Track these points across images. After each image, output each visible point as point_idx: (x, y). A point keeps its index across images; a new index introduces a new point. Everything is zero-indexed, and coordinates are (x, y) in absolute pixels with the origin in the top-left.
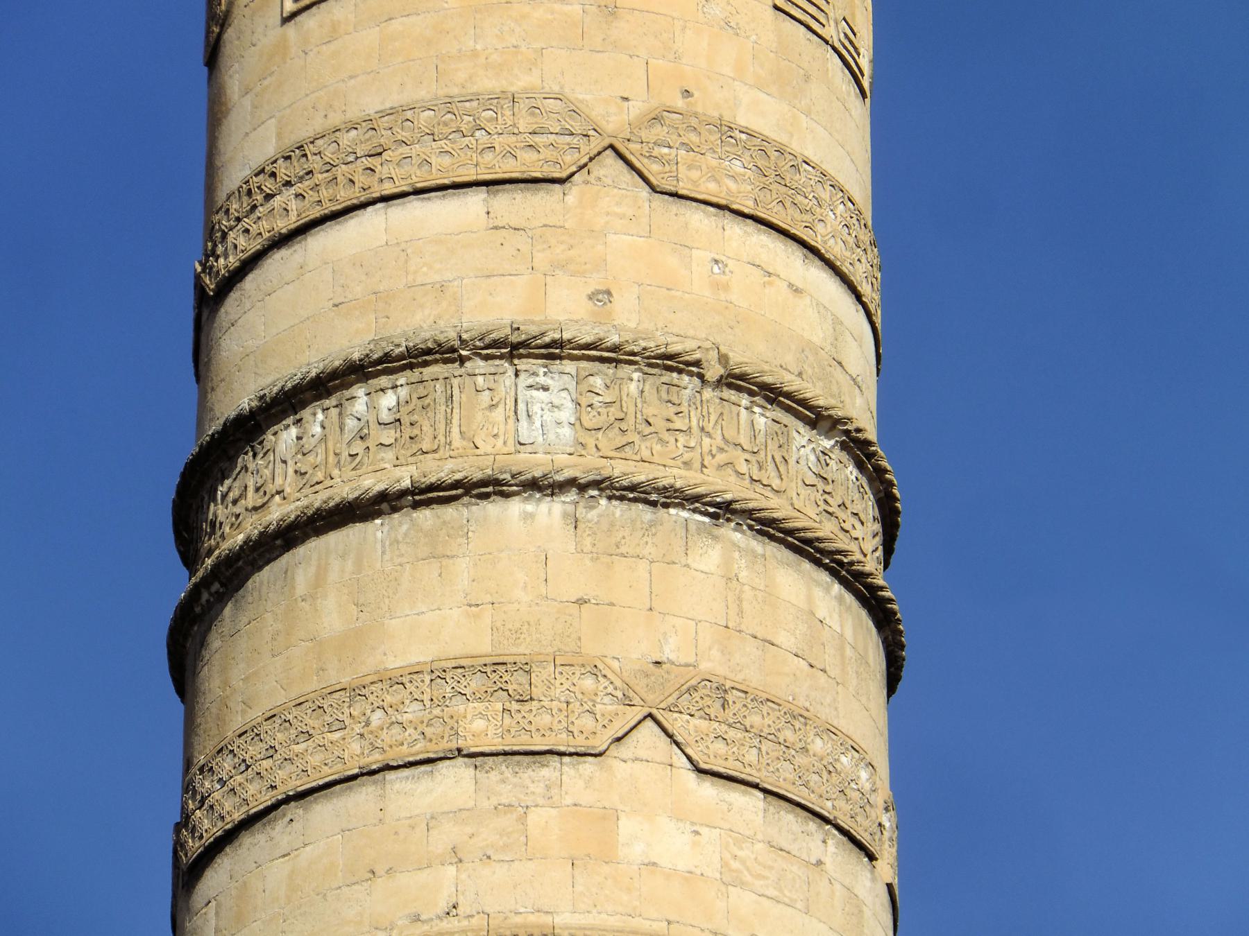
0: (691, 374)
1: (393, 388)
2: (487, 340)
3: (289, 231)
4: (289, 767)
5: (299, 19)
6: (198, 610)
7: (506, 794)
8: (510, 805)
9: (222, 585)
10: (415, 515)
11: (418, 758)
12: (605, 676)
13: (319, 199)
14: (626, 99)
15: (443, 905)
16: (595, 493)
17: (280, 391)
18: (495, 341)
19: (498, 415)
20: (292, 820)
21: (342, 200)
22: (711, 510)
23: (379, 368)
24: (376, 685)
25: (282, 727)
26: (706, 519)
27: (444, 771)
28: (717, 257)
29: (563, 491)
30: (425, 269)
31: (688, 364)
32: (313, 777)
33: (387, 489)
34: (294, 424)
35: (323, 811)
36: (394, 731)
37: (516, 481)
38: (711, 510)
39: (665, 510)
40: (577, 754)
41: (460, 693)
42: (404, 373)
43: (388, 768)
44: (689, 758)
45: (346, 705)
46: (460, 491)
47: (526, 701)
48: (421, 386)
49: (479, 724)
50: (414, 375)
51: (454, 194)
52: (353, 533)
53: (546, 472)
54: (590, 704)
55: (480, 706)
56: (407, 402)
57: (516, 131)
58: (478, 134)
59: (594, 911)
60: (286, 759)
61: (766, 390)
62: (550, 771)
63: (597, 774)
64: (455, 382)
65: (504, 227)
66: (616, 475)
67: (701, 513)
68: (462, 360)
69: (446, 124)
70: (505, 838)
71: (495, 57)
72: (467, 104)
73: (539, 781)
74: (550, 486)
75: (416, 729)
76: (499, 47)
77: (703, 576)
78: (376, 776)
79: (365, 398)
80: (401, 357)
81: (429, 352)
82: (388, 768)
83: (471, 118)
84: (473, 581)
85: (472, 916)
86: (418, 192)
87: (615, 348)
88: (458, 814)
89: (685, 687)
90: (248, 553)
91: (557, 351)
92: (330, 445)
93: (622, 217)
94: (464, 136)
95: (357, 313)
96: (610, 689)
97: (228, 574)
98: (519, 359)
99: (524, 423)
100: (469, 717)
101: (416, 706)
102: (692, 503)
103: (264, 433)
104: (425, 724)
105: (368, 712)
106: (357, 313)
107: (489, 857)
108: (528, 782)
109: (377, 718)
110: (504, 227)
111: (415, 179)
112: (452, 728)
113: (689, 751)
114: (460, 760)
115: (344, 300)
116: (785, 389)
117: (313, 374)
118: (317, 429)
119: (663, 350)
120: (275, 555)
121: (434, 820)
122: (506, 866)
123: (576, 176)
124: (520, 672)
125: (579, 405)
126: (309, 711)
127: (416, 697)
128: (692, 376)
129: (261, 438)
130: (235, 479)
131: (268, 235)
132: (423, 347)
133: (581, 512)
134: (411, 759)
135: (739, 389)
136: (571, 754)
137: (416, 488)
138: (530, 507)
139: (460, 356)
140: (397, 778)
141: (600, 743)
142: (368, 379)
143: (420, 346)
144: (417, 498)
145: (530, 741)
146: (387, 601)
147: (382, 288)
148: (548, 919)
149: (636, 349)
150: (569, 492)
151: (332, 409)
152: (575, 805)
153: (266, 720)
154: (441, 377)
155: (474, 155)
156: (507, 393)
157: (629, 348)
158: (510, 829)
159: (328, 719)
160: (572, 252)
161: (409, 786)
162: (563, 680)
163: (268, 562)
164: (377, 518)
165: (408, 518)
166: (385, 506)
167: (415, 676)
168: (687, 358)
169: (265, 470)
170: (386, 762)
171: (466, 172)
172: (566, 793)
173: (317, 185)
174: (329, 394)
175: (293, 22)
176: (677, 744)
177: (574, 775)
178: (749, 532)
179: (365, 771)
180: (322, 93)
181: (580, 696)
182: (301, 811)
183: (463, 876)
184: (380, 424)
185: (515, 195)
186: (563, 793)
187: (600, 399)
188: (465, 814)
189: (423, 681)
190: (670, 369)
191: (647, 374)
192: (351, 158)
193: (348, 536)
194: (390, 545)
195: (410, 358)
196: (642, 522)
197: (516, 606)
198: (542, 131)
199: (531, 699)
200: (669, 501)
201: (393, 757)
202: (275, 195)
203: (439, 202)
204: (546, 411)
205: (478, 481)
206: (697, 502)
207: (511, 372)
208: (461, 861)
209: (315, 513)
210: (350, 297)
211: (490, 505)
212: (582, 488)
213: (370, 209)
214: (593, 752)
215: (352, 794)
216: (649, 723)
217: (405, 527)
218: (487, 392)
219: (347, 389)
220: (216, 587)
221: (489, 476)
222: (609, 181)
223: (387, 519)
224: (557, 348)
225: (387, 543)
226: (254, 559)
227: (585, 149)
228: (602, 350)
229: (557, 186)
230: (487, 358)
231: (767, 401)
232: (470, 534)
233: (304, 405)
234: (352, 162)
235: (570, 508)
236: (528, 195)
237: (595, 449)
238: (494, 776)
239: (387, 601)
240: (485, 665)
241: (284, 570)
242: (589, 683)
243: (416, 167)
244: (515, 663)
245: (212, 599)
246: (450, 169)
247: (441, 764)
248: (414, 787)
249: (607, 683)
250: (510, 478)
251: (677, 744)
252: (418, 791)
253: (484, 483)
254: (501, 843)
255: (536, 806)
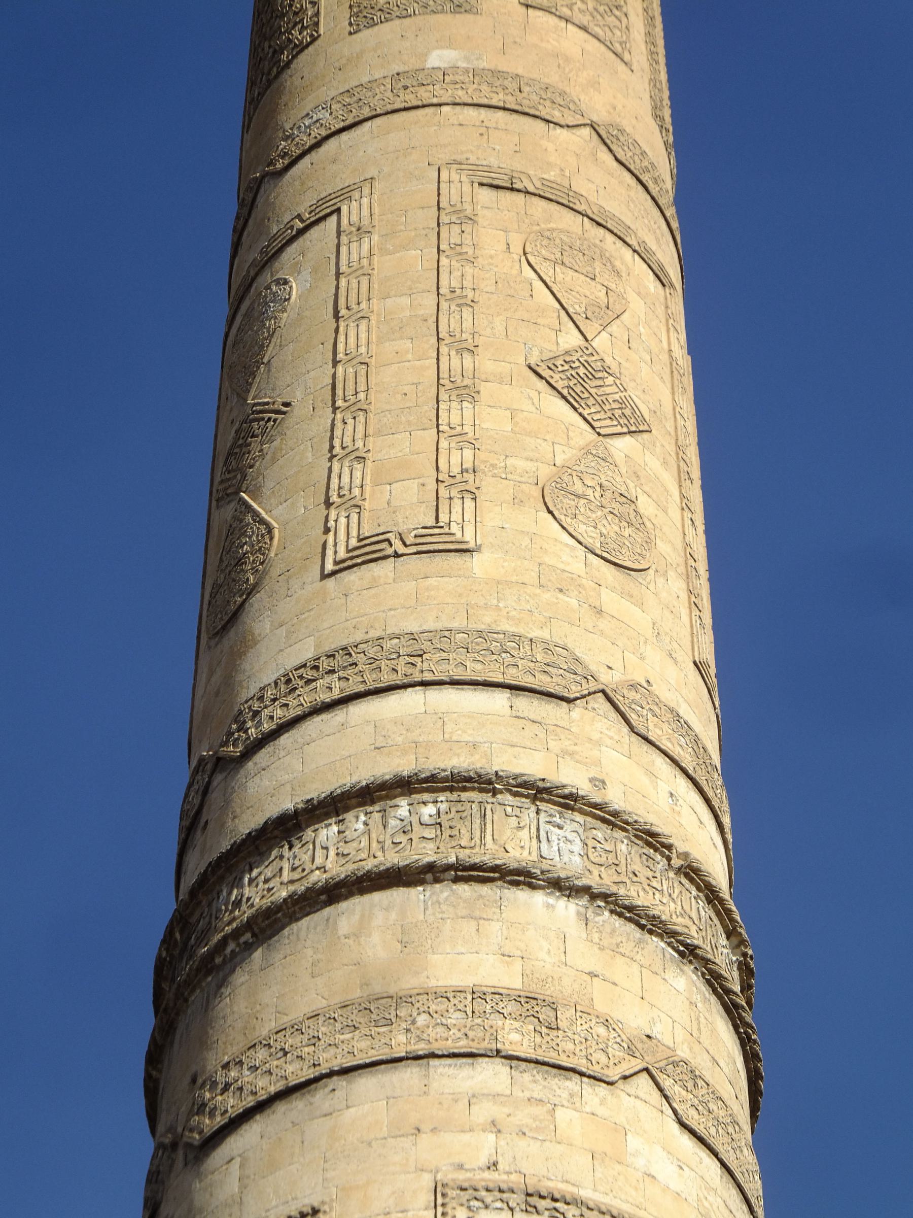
0: (663, 855)
1: (433, 802)
2: (519, 780)
3: (332, 700)
4: (332, 1050)
5: (338, 576)
6: (218, 960)
7: (537, 1092)
8: (541, 1100)
9: (254, 935)
10: (454, 887)
11: (462, 1051)
12: (614, 1029)
13: (362, 680)
14: (610, 668)
15: (483, 1161)
16: (602, 904)
17: (329, 796)
18: (525, 782)
19: (524, 834)
20: (334, 1090)
21: (385, 681)
22: (681, 948)
23: (424, 785)
24: (422, 997)
25: (326, 1023)
26: (676, 955)
27: (484, 1065)
28: (672, 792)
29: (578, 895)
30: (459, 732)
31: (664, 845)
32: (358, 1057)
33: (435, 862)
34: (335, 823)
35: (365, 1083)
36: (438, 1030)
37: (545, 877)
38: (681, 948)
39: (649, 936)
40: (595, 1078)
41: (498, 1011)
42: (445, 793)
43: (433, 1056)
44: (675, 1112)
45: (393, 1008)
46: (497, 875)
47: (554, 1029)
48: (459, 804)
49: (515, 1037)
50: (454, 796)
51: (484, 690)
52: (397, 895)
53: (569, 876)
54: (605, 1045)
55: (517, 1024)
56: (447, 813)
57: (534, 660)
58: (504, 655)
59: (611, 1195)
60: (330, 1045)
61: (708, 890)
62: (573, 1084)
63: (609, 1097)
64: (489, 807)
65: (524, 718)
66: (621, 894)
67: (673, 948)
68: (495, 792)
69: (477, 644)
70: (537, 1123)
71: (513, 613)
72: (495, 635)
73: (564, 1089)
74: (569, 889)
75: (459, 1030)
76: (518, 608)
77: (675, 992)
78: (421, 1062)
79: (408, 807)
80: (445, 780)
81: (469, 780)
82: (433, 1056)
83: (499, 644)
84: (507, 939)
85: (511, 1173)
86: (454, 683)
87: (616, 814)
88: (495, 1097)
89: (670, 1059)
90: (290, 905)
91: (572, 803)
92: (374, 836)
93: (611, 738)
94: (493, 654)
95: (399, 754)
96: (618, 1040)
97: (263, 925)
98: (541, 802)
99: (544, 845)
100: (507, 1029)
101: (459, 1015)
102: (669, 938)
103: (304, 831)
104: (468, 1028)
105: (415, 1014)
106: (399, 754)
107: (524, 1134)
108: (555, 1087)
109: (422, 1020)
110: (524, 718)
111: (452, 673)
112: (492, 1034)
113: (675, 1105)
114: (498, 1060)
115: (385, 745)
116: (721, 895)
117: (364, 783)
118: (360, 826)
119: (649, 827)
120: (315, 909)
121: (475, 1099)
122: (539, 1143)
123: (578, 701)
124: (548, 1008)
125: (586, 845)
126: (355, 1012)
127: (459, 1008)
128: (663, 857)
129: (301, 834)
130: (267, 867)
131: (309, 704)
132: (466, 775)
133: (590, 914)
134: (456, 1051)
135: (692, 880)
136: (590, 1077)
137: (460, 865)
138: (551, 900)
139: (494, 788)
140: (440, 1065)
141: (613, 1074)
142: (411, 794)
143: (463, 774)
144: (460, 873)
145: (558, 1057)
146: (429, 941)
147: (421, 740)
148: (574, 1190)
149: (630, 820)
150: (582, 897)
151: (375, 813)
152: (593, 1114)
153: (308, 1019)
154: (477, 801)
155: (502, 667)
156: (530, 821)
157: (625, 817)
158: (542, 1118)
159: (374, 1017)
160: (576, 748)
161: (451, 1071)
162: (583, 1022)
163: (307, 915)
164: (420, 886)
165: (448, 889)
166: (429, 877)
167: (458, 994)
168: (664, 840)
169: (304, 856)
170: (432, 1051)
171: (495, 676)
172: (586, 1103)
173: (360, 672)
174: (373, 802)
175: (333, 578)
176: (666, 1097)
177: (593, 1094)
178: (701, 978)
179: (411, 1056)
180: (363, 619)
181: (596, 1037)
182: (344, 1083)
183: (502, 1143)
184: (421, 824)
185: (533, 700)
186: (584, 1103)
187: (602, 846)
188: (502, 1099)
189: (466, 998)
190: (649, 845)
191: (633, 842)
192: (394, 656)
193: (392, 896)
194: (432, 904)
195: (452, 782)
196: (634, 937)
197: (542, 963)
198: (554, 665)
199: (558, 1029)
200: (654, 929)
201: (437, 1047)
202: (317, 679)
203: (471, 692)
204: (561, 841)
205: (514, 869)
206: (673, 937)
207: (533, 808)
208: (499, 1131)
209: (364, 874)
210: (391, 743)
211: (519, 892)
212: (594, 897)
213: (409, 690)
214: (607, 1080)
215: (397, 1073)
216: (645, 1075)
217: (445, 894)
218: (515, 818)
219: (391, 800)
220: (248, 936)
221: (524, 867)
222: (601, 712)
223: (429, 887)
224: (572, 801)
225: (430, 903)
226: (294, 912)
227: (585, 685)
228: (605, 812)
229: (564, 704)
230: (516, 794)
231: (706, 899)
232: (502, 907)
233: (347, 809)
234: (394, 659)
235: (583, 910)
236: (543, 703)
237: (598, 878)
238: (527, 1077)
239: (429, 941)
240: (520, 996)
241: (326, 918)
242: (602, 1030)
243: (453, 666)
244: (544, 1000)
245: (237, 950)
246: (482, 671)
247: (480, 1060)
248: (456, 1072)
249: (616, 1035)
250: (539, 873)
251: (666, 1097)
252: (460, 1076)
253: (518, 872)
254: (534, 1126)
255: (563, 1106)
